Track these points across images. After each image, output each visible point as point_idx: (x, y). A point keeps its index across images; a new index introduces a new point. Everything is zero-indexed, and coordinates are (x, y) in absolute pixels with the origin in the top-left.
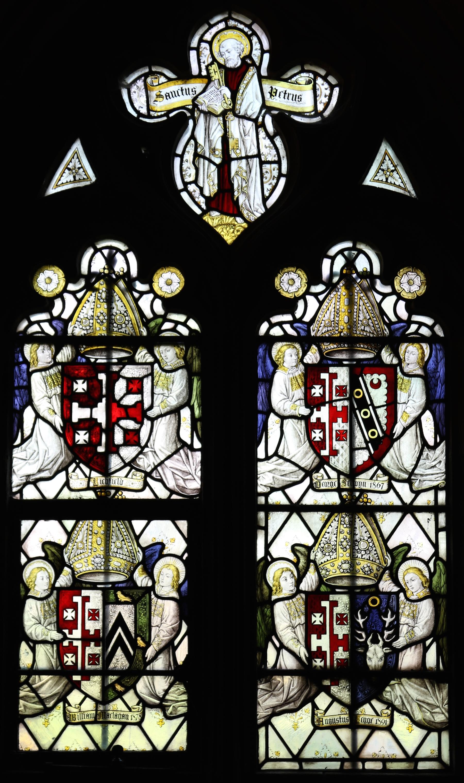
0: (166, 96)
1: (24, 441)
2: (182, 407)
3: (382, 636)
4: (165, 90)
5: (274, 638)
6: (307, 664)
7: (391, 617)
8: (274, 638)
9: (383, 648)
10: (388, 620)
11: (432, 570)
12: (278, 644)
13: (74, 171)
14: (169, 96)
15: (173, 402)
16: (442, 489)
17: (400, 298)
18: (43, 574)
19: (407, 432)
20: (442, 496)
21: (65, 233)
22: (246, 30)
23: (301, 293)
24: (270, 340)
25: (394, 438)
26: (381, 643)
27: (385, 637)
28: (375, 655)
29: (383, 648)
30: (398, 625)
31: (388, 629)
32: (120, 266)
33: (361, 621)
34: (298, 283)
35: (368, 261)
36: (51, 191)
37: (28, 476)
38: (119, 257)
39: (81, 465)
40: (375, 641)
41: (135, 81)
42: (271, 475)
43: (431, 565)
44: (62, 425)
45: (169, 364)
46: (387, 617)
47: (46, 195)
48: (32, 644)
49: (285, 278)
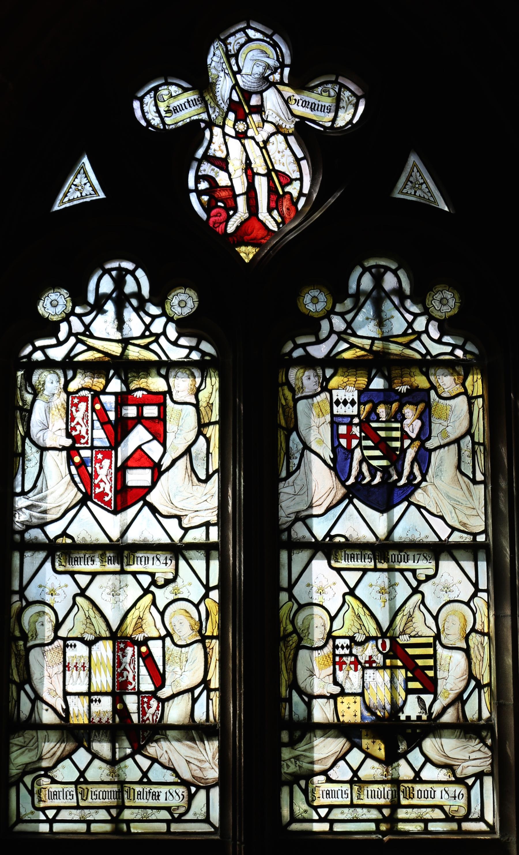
0: (174, 110)
1: (290, 474)
2: (463, 437)
4: (175, 103)
5: (27, 687)
6: (64, 716)
8: (27, 687)
12: (32, 696)
13: (83, 186)
14: (177, 109)
15: (454, 433)
16: (214, 525)
20: (214, 535)
21: (72, 253)
22: (268, 40)
24: (32, 366)
25: (162, 470)
32: (130, 287)
35: (139, 282)
36: (56, 208)
37: (298, 512)
39: (355, 501)
41: (145, 95)
43: (202, 608)
44: (332, 457)
45: (446, 390)
47: (51, 211)
48: (306, 699)
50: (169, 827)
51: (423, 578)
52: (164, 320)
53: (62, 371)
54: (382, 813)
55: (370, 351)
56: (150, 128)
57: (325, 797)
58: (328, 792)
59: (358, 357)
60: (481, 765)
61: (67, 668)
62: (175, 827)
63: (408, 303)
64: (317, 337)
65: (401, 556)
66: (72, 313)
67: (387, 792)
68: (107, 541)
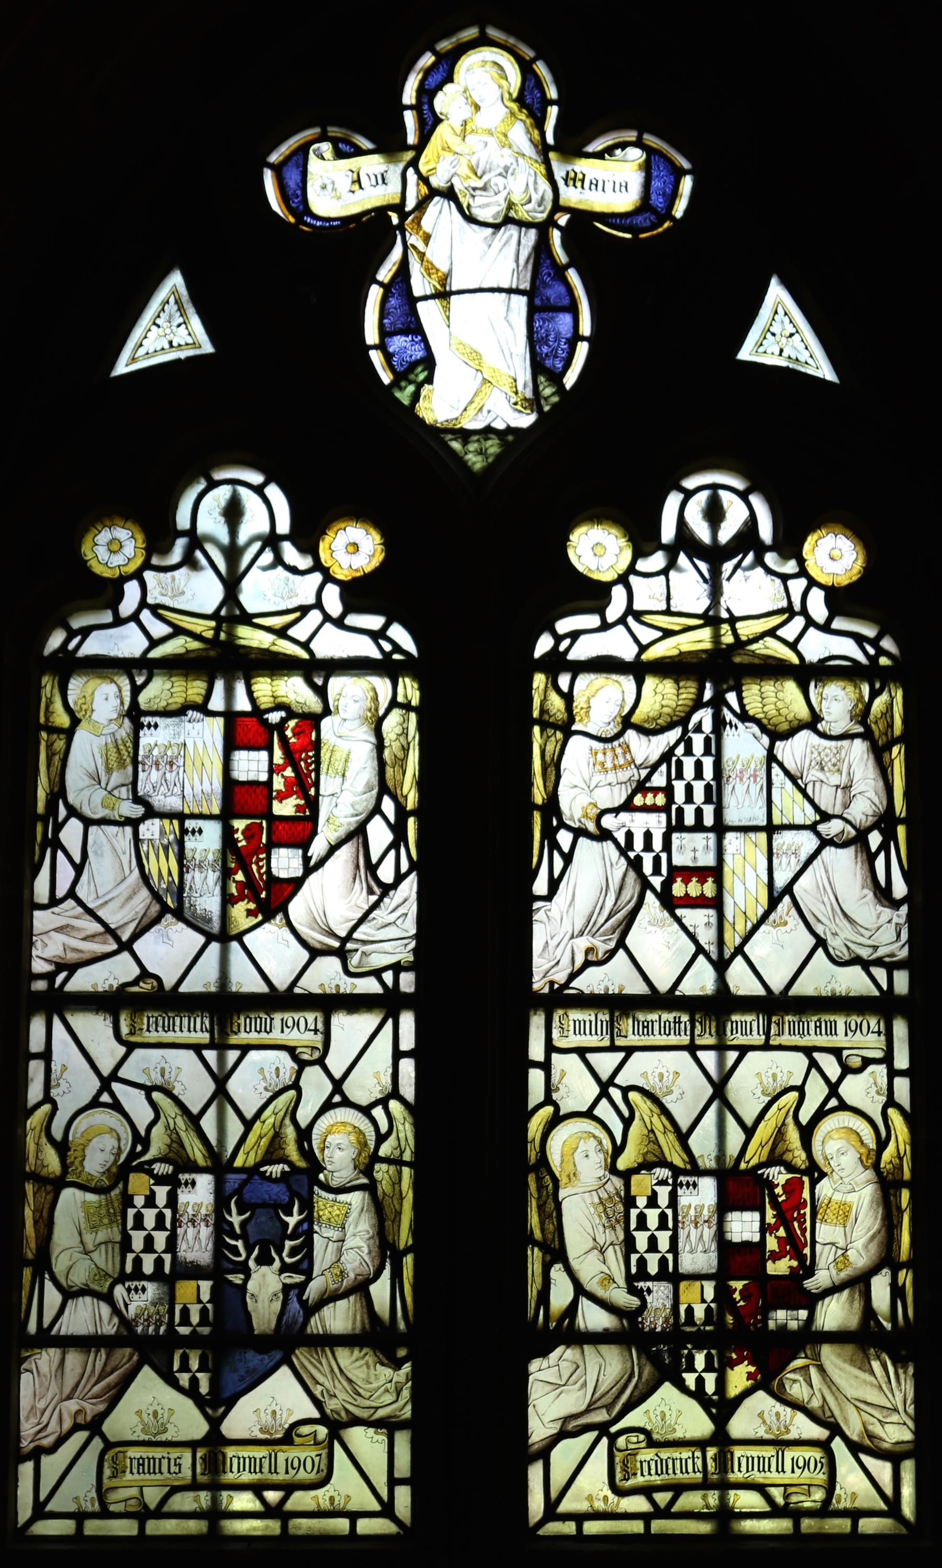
3: (280, 1252)
7: (300, 1213)
9: (280, 1275)
10: (292, 1221)
11: (619, 1142)
13: (166, 331)
16: (407, 969)
17: (328, 578)
18: (109, 1142)
19: (337, 853)
20: (407, 982)
21: (150, 451)
23: (132, 568)
26: (277, 1264)
27: (284, 1254)
28: (265, 1286)
29: (280, 1275)
30: (310, 1233)
31: (292, 1237)
33: (236, 1219)
34: (128, 549)
35: (268, 509)
38: (250, 499)
40: (266, 1260)
42: (60, 938)
46: (291, 1215)
49: (104, 536)
50: (647, 1527)
51: (856, 1062)
52: (317, 577)
53: (631, 677)
54: (263, 1500)
55: (213, 642)
56: (643, 236)
57: (135, 1471)
58: (141, 1461)
59: (188, 651)
60: (58, 1409)
61: (680, 1225)
62: (658, 1526)
63: (770, 559)
64: (116, 613)
65: (261, 1019)
66: (147, 565)
67: (739, 1459)
68: (264, 989)
